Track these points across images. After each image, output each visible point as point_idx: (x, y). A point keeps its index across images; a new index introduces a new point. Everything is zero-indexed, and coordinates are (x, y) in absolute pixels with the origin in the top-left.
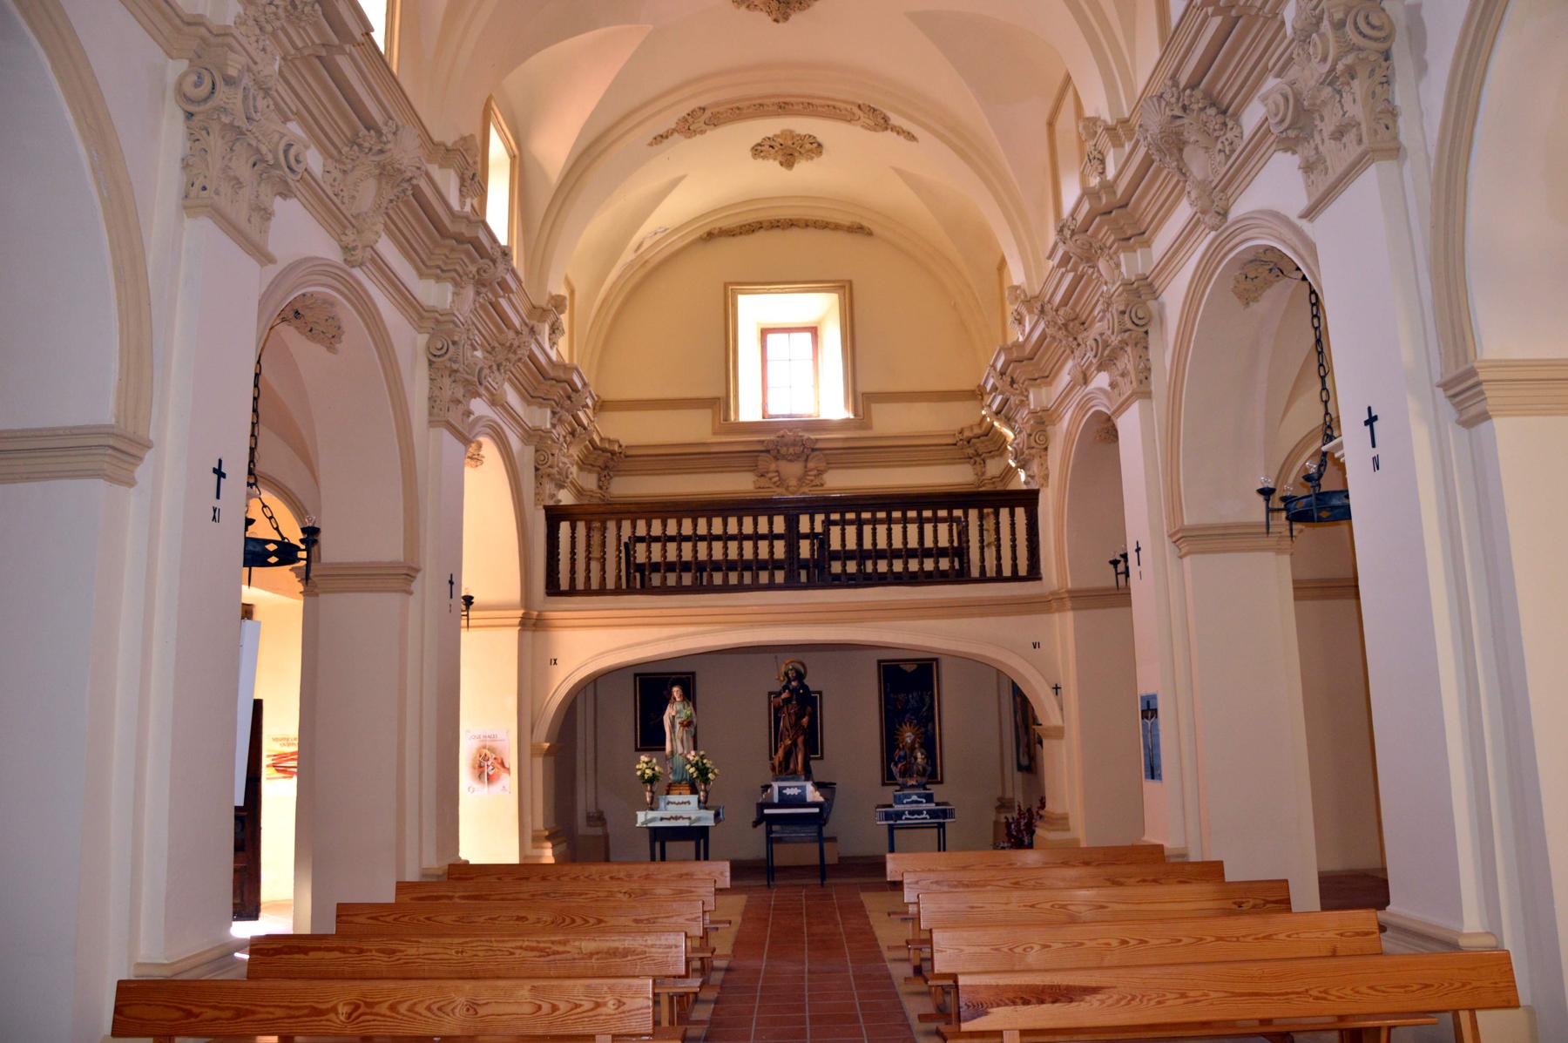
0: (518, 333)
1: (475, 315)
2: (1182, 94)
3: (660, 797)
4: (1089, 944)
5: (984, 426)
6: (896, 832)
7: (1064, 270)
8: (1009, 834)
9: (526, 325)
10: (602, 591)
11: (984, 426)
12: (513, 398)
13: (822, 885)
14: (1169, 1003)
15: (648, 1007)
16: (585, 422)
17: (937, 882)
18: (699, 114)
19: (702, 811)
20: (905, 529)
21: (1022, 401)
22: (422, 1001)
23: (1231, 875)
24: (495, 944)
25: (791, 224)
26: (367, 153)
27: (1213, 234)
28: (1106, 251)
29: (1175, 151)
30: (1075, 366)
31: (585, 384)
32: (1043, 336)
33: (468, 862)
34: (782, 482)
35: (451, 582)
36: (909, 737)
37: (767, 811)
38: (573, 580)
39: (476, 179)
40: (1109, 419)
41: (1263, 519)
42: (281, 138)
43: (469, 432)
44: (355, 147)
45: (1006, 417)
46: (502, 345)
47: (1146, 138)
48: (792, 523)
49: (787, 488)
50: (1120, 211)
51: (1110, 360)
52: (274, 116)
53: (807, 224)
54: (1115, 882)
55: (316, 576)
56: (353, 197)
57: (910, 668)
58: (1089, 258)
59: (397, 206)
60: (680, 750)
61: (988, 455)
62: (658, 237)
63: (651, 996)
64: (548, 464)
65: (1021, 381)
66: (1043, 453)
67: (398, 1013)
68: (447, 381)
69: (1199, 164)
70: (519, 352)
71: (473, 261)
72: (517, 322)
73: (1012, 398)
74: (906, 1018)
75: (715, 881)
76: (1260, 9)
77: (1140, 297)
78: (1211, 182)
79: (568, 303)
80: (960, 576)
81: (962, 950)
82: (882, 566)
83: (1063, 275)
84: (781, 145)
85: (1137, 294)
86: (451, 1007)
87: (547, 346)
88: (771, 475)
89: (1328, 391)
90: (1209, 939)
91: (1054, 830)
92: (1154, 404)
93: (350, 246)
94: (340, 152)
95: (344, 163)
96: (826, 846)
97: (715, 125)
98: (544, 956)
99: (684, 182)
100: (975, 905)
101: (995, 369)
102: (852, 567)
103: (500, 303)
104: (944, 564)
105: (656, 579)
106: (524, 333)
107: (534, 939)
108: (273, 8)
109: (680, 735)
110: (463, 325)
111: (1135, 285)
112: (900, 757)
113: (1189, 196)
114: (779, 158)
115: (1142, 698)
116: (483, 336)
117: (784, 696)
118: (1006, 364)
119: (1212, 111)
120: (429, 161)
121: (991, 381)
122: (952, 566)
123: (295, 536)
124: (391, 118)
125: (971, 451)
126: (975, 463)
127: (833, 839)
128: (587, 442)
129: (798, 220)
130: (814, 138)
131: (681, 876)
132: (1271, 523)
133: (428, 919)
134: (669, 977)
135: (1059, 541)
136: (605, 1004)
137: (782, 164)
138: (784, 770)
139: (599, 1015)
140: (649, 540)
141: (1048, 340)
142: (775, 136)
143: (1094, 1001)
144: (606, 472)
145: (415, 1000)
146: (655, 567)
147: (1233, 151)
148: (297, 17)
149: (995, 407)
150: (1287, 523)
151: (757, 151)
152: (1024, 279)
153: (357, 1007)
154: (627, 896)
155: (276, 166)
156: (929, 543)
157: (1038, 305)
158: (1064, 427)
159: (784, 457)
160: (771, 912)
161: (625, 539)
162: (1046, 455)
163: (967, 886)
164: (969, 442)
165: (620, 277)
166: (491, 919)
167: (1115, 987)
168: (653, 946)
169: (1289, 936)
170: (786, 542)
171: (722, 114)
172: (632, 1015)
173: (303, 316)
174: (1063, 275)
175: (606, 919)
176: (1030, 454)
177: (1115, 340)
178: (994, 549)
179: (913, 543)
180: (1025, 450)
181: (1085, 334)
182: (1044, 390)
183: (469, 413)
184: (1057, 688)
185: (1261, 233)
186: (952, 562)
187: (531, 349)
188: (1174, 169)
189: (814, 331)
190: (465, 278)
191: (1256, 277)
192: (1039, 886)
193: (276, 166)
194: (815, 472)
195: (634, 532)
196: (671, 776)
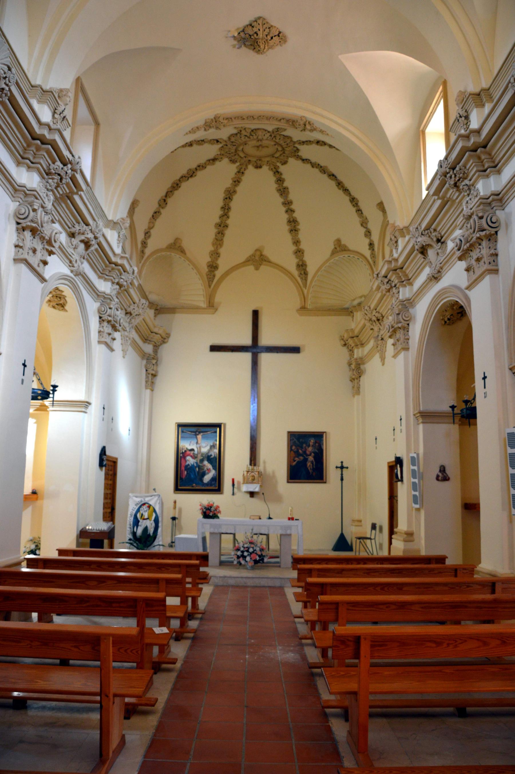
7: (436, 197)
118: (388, 272)
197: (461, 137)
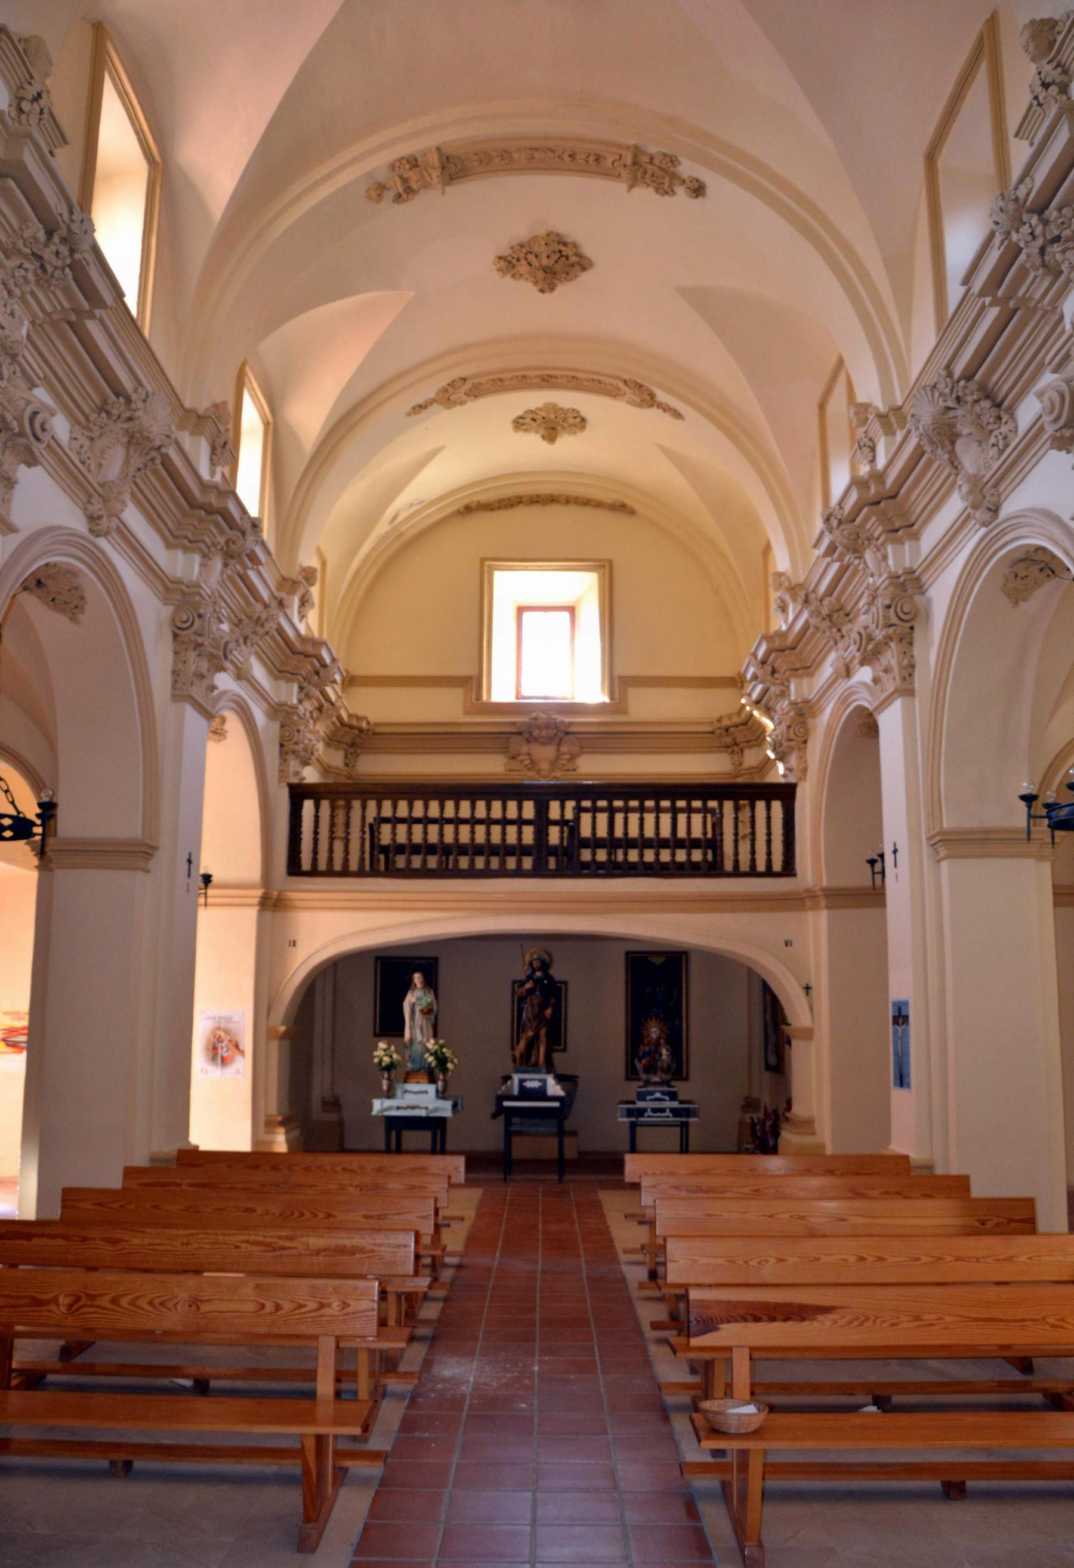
0: (266, 606)
1: (221, 586)
2: (956, 385)
4: (825, 1259)
5: (743, 715)
6: (639, 1130)
7: (829, 559)
9: (275, 598)
10: (345, 873)
12: (259, 672)
14: (903, 1325)
15: (373, 1310)
16: (333, 697)
17: (676, 1187)
18: (460, 384)
20: (657, 819)
22: (144, 1296)
23: (977, 1191)
24: (221, 1237)
25: (552, 500)
26: (115, 421)
27: (984, 530)
28: (874, 542)
29: (947, 443)
30: (838, 658)
31: (334, 660)
32: (806, 626)
33: (197, 1147)
34: (533, 765)
35: (190, 861)
36: (654, 1032)
37: (506, 1104)
38: (315, 860)
39: (227, 447)
40: (870, 715)
41: (1024, 824)
42: (27, 405)
43: (213, 706)
44: (104, 414)
46: (249, 617)
47: (917, 429)
48: (542, 809)
49: (538, 772)
50: (889, 501)
51: (874, 655)
52: (20, 381)
54: (857, 1194)
55: (52, 851)
56: (100, 465)
57: (658, 961)
58: (857, 551)
59: (145, 474)
60: (419, 1037)
61: (746, 744)
62: (414, 508)
63: (376, 1298)
65: (782, 671)
66: (802, 746)
67: (119, 1306)
68: (192, 655)
69: (970, 457)
71: (222, 532)
74: (638, 1324)
75: (449, 1177)
76: (1039, 302)
77: (906, 591)
78: (983, 477)
79: (319, 575)
80: (713, 869)
81: (695, 1261)
82: (633, 856)
83: (828, 565)
85: (902, 587)
86: (175, 1301)
87: (296, 619)
88: (522, 757)
90: (949, 1259)
91: (797, 1133)
92: (917, 703)
93: (95, 516)
94: (87, 419)
95: (91, 430)
96: (568, 1141)
97: (476, 396)
98: (271, 1251)
100: (713, 1213)
101: (756, 658)
102: (602, 855)
103: (248, 576)
104: (697, 855)
105: (401, 861)
106: (272, 605)
107: (261, 1233)
108: (23, 272)
109: (420, 1023)
110: (210, 597)
111: (902, 579)
112: (644, 1053)
113: (960, 490)
114: (542, 432)
115: (894, 1004)
116: (230, 608)
117: (528, 986)
118: (768, 654)
119: (986, 404)
120: (181, 427)
121: (752, 670)
122: (705, 860)
123: (30, 810)
124: (141, 384)
125: (728, 740)
126: (732, 752)
127: (574, 1133)
129: (559, 496)
130: (578, 412)
131: (414, 1170)
132: (1032, 828)
133: (155, 1207)
134: (398, 1276)
135: (815, 839)
136: (329, 1305)
137: (543, 438)
138: (526, 1062)
139: (322, 1316)
140: (395, 821)
143: (826, 1321)
144: (352, 750)
145: (137, 1294)
146: (400, 849)
147: (1007, 446)
148: (47, 281)
150: (1049, 830)
151: (519, 424)
153: (78, 1299)
154: (358, 1189)
155: (22, 434)
156: (682, 833)
157: (802, 594)
158: (826, 719)
159: (536, 740)
160: (507, 1207)
161: (370, 819)
162: (805, 748)
163: (707, 1192)
164: (727, 730)
165: (373, 549)
166: (219, 1209)
167: (848, 1307)
168: (380, 1245)
169: (1030, 1259)
170: (535, 828)
172: (356, 1318)
173: (45, 585)
174: (828, 565)
175: (334, 1213)
176: (789, 747)
177: (879, 635)
178: (748, 843)
179: (666, 832)
180: (783, 741)
181: (849, 626)
182: (805, 681)
183: (213, 688)
184: (808, 989)
185: (1033, 532)
186: (705, 854)
188: (945, 461)
189: (571, 610)
190: (213, 549)
191: (1026, 577)
192: (780, 1196)
193: (22, 434)
194: (568, 756)
195: (379, 813)
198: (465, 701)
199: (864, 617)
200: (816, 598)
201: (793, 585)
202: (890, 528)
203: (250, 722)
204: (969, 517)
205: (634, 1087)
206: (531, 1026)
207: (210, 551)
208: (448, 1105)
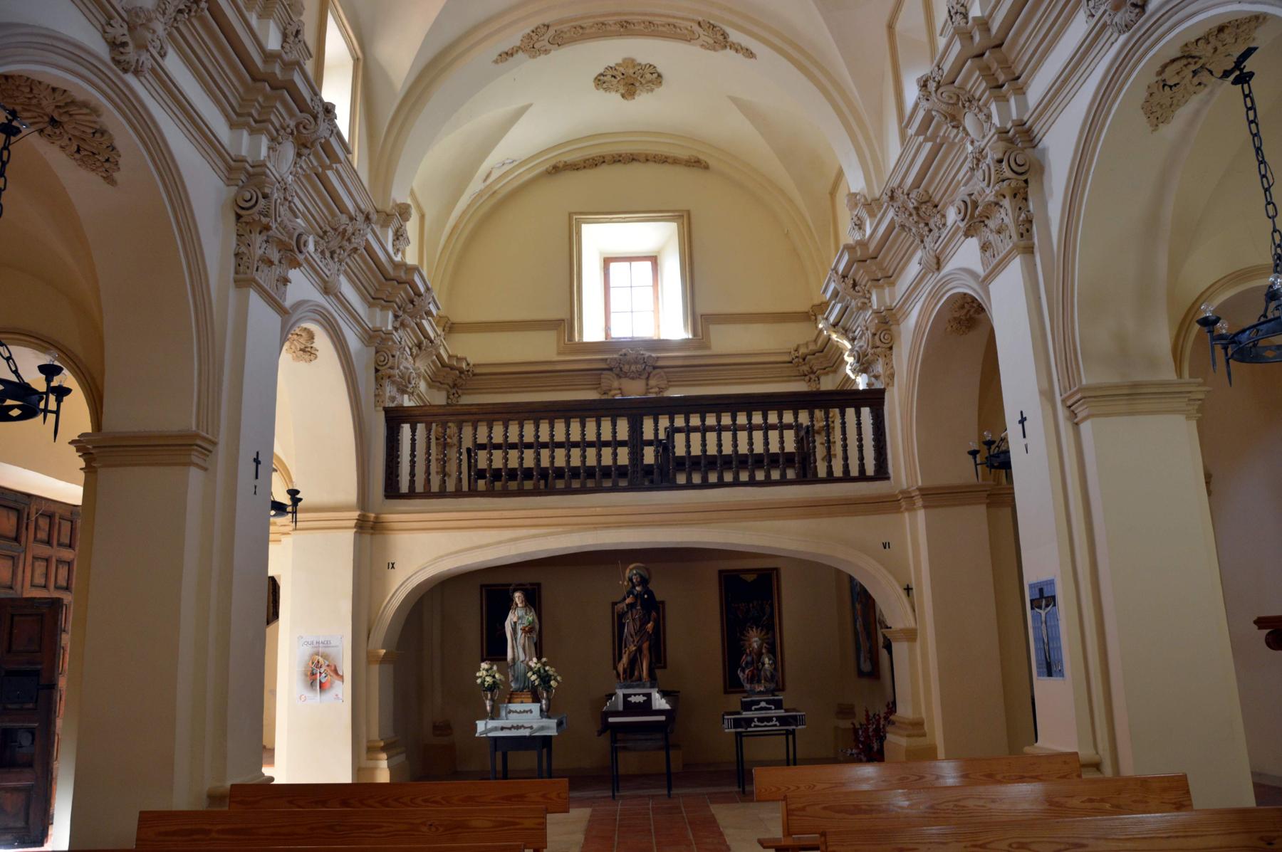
0: (352, 219)
3: (501, 705)
7: (921, 138)
8: (857, 740)
9: (361, 211)
11: (819, 343)
13: (669, 795)
18: (543, 30)
19: (544, 720)
21: (864, 304)
25: (633, 158)
27: (1123, 38)
28: (975, 103)
31: (428, 289)
35: (257, 461)
37: (611, 720)
45: (843, 328)
46: (335, 230)
48: (636, 429)
53: (648, 159)
57: (750, 578)
58: (955, 120)
60: (522, 657)
61: (822, 371)
62: (507, 168)
64: (388, 366)
65: (864, 283)
70: (353, 240)
71: (292, 115)
72: (350, 206)
73: (853, 303)
80: (807, 475)
84: (623, 74)
89: (1274, 205)
93: (118, 42)
96: (673, 753)
99: (531, 109)
101: (837, 273)
106: (358, 219)
109: (522, 641)
117: (628, 601)
118: (849, 266)
125: (805, 368)
128: (435, 357)
129: (639, 154)
130: (655, 67)
138: (630, 677)
141: (896, 230)
142: (617, 64)
144: (454, 391)
149: (832, 319)
151: (600, 81)
152: (864, 183)
158: (911, 322)
159: (626, 375)
164: (804, 359)
171: (566, 33)
176: (875, 354)
177: (990, 194)
184: (908, 590)
187: (367, 240)
190: (282, 132)
196: (513, 685)
197: (1018, 133)
198: (558, 341)
199: (963, 188)
200: (903, 193)
201: (869, 201)
202: (995, 84)
203: (339, 340)
204: (1104, 26)
205: (735, 700)
206: (634, 641)
207: (278, 134)
208: (553, 723)
